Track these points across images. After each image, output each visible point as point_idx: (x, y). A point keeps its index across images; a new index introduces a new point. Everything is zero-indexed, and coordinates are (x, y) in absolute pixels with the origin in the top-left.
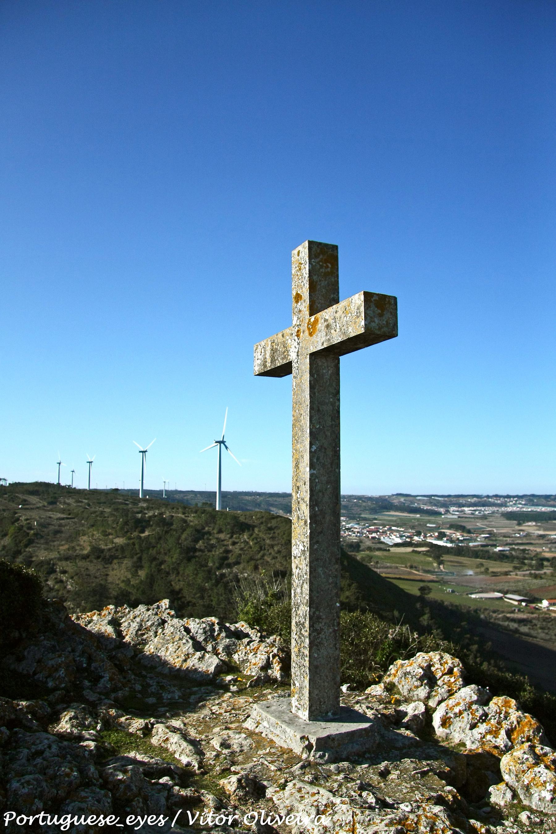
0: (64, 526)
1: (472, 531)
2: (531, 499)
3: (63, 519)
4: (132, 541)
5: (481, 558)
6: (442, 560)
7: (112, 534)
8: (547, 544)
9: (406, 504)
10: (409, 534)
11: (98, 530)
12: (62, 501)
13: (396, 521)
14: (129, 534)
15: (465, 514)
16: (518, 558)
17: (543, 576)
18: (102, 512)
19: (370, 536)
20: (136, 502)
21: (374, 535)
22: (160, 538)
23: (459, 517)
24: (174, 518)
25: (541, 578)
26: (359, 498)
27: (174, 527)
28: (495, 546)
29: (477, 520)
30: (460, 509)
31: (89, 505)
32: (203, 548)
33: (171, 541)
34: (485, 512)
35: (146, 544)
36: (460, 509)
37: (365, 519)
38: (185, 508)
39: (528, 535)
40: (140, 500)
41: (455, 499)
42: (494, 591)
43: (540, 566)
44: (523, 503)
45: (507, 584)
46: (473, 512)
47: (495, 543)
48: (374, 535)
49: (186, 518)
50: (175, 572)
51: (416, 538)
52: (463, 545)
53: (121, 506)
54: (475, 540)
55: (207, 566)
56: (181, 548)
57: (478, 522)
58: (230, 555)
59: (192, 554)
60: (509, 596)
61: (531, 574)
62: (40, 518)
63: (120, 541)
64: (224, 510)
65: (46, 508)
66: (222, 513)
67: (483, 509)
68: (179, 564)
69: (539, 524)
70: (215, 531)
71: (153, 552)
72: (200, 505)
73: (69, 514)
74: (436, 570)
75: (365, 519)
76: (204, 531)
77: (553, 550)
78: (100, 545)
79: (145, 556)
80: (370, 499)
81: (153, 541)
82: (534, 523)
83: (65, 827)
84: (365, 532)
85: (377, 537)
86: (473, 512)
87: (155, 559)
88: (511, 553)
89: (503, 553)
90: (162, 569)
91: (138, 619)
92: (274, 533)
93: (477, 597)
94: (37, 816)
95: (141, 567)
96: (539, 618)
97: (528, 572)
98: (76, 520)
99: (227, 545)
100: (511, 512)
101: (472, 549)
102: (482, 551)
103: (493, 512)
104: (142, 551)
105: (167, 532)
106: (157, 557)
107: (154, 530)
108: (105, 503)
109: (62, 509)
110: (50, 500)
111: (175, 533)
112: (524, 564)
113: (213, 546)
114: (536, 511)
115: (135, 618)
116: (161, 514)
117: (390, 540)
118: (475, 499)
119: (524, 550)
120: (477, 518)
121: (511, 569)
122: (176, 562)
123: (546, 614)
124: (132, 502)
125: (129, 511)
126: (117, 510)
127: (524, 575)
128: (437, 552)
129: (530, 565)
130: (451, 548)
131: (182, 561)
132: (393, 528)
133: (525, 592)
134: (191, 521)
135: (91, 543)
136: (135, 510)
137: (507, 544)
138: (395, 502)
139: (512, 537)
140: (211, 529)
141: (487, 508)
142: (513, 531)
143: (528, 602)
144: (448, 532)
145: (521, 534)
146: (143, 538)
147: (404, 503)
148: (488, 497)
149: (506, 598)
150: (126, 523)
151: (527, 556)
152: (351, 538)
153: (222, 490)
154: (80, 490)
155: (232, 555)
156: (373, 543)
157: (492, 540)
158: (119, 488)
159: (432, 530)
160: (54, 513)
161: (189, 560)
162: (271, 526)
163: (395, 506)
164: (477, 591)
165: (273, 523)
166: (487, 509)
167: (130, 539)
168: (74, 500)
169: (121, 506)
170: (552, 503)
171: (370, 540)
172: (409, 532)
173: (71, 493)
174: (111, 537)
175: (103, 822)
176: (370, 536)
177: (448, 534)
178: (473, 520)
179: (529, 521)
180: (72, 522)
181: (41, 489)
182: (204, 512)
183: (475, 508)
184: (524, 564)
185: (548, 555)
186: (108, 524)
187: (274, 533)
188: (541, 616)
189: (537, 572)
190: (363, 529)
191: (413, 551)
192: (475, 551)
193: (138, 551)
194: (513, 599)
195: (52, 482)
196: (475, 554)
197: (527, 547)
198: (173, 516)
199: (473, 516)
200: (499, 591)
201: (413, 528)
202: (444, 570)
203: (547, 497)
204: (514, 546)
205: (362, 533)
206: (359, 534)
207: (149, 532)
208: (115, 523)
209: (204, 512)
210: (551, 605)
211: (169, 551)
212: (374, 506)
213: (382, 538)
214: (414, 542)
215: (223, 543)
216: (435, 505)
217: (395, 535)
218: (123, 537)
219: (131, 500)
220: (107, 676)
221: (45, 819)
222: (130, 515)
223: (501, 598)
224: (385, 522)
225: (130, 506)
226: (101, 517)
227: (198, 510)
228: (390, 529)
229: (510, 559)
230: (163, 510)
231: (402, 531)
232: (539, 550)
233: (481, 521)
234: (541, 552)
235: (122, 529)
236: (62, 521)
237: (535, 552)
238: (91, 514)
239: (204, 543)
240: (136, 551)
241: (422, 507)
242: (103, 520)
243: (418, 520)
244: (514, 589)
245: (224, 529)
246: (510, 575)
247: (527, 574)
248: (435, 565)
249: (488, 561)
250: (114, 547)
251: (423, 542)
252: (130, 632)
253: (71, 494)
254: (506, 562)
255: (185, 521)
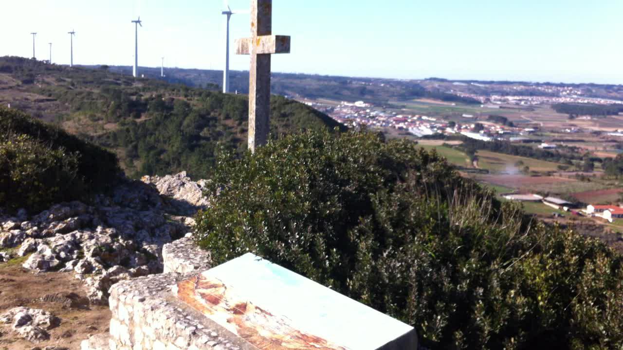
0: (44, 110)
1: (514, 123)
2: (589, 89)
3: (42, 101)
4: (126, 127)
5: (522, 155)
6: (476, 156)
7: (102, 119)
8: (602, 142)
9: (441, 91)
10: (441, 125)
11: (85, 114)
12: (40, 80)
13: (427, 109)
14: (122, 119)
15: (508, 104)
16: (565, 157)
17: (591, 179)
18: (90, 94)
19: (397, 126)
20: (130, 82)
21: (401, 125)
22: (158, 124)
23: (501, 107)
24: (174, 102)
25: (589, 180)
26: (388, 82)
27: (174, 112)
28: (540, 142)
29: (521, 111)
30: (503, 98)
31: (73, 85)
32: (208, 136)
33: (171, 127)
34: (532, 103)
35: (142, 130)
36: (503, 98)
37: (392, 107)
38: (187, 90)
39: (580, 131)
40: (133, 80)
41: (498, 86)
42: (533, 192)
43: (590, 167)
44: (579, 93)
45: (548, 186)
46: (519, 102)
47: (540, 138)
48: (401, 125)
49: (188, 102)
50: (176, 162)
51: (449, 130)
52: (502, 139)
53: (111, 87)
54: (517, 135)
55: (212, 156)
56: (183, 135)
57: (523, 114)
58: (238, 144)
59: (195, 142)
60: (549, 199)
61: (577, 176)
62: (14, 99)
63: (112, 127)
64: (231, 93)
65: (21, 88)
66: (229, 97)
67: (530, 98)
68: (180, 153)
69: (595, 119)
70: (222, 117)
71: (151, 140)
72: (204, 86)
73: (50, 95)
74: (468, 167)
75: (392, 107)
76: (209, 116)
77: (608, 149)
78: (88, 131)
79: (141, 145)
80: (399, 83)
81: (151, 127)
82: (589, 118)
84: (392, 121)
85: (405, 127)
86: (519, 102)
87: (152, 148)
88: (557, 151)
89: (550, 150)
90: (161, 159)
91: (167, 183)
92: (288, 120)
93: (513, 198)
95: (137, 157)
96: (581, 225)
97: (574, 173)
98: (58, 102)
99: (236, 133)
100: (563, 103)
101: (512, 144)
102: (524, 147)
103: (542, 103)
104: (138, 139)
105: (166, 117)
106: (156, 146)
107: (151, 115)
108: (92, 82)
109: (41, 89)
110: (25, 78)
111: (175, 118)
112: (571, 163)
113: (219, 134)
114: (594, 103)
115: (165, 182)
116: (160, 96)
117: (419, 131)
118: (522, 87)
119: (572, 149)
120: (522, 109)
121: (555, 169)
122: (177, 151)
123: (590, 220)
124: (125, 82)
125: (121, 92)
126: (107, 91)
127: (569, 177)
128: (471, 146)
129: (578, 166)
130: (488, 142)
131: (183, 151)
132: (424, 118)
133: (568, 195)
134: (194, 105)
135: (78, 129)
136: (129, 91)
137: (554, 141)
138: (429, 87)
139: (561, 133)
140: (217, 114)
141: (535, 98)
142: (564, 125)
143: (572, 206)
144: (486, 124)
145: (573, 129)
146: (138, 124)
147: (438, 90)
148: (538, 84)
149: (545, 201)
150: (119, 107)
151: (576, 155)
152: (375, 127)
153: (231, 68)
154: (60, 66)
155: (241, 144)
156: (399, 134)
157: (538, 135)
158: (108, 64)
159: (468, 121)
160: (32, 94)
161: (192, 149)
162: (285, 113)
163: (427, 92)
164: (513, 192)
165: (287, 109)
166: (534, 99)
167: (123, 124)
168: (54, 79)
169: (111, 87)
170: (614, 94)
171: (396, 130)
172: (442, 123)
173: (50, 70)
174: (100, 122)
176: (397, 126)
177: (486, 126)
178: (517, 111)
179: (583, 114)
180: (53, 104)
181: (13, 65)
182: (208, 95)
183: (521, 98)
184: (571, 163)
185: (601, 155)
186: (97, 108)
187: (288, 120)
188: (584, 223)
189: (585, 174)
190: (389, 117)
191: (445, 145)
192: (515, 146)
193: (133, 139)
194: (554, 203)
195: (25, 56)
196: (516, 150)
197: (577, 145)
198: (173, 99)
199: (517, 107)
200: (538, 193)
201: (446, 118)
202: (477, 167)
203: (609, 87)
204: (562, 143)
205: (388, 123)
206: (384, 124)
207: (146, 117)
208: (105, 106)
209: (208, 95)
210: (597, 211)
211: (169, 138)
212: (404, 91)
213: (410, 129)
214: (446, 134)
215: (230, 130)
216: (475, 92)
217: (426, 126)
218: (115, 122)
219: (124, 80)
220: (159, 204)
222: (123, 97)
223: (540, 201)
224: (416, 111)
225: (123, 86)
226: (88, 99)
227: (203, 92)
228: (420, 119)
229: (555, 158)
230: (162, 91)
231: (433, 121)
232: (591, 148)
233: (526, 113)
234: (593, 152)
235: (114, 113)
236: (42, 104)
237: (586, 152)
238: (76, 95)
239: (209, 131)
240: (131, 138)
241: (459, 94)
242: (90, 103)
243: (452, 109)
244: (557, 191)
245: (231, 114)
246: (554, 176)
247: (573, 176)
248: (468, 160)
249: (531, 159)
250: (106, 134)
251: (456, 135)
252: (163, 189)
253: (50, 72)
254: (550, 161)
255: (188, 105)
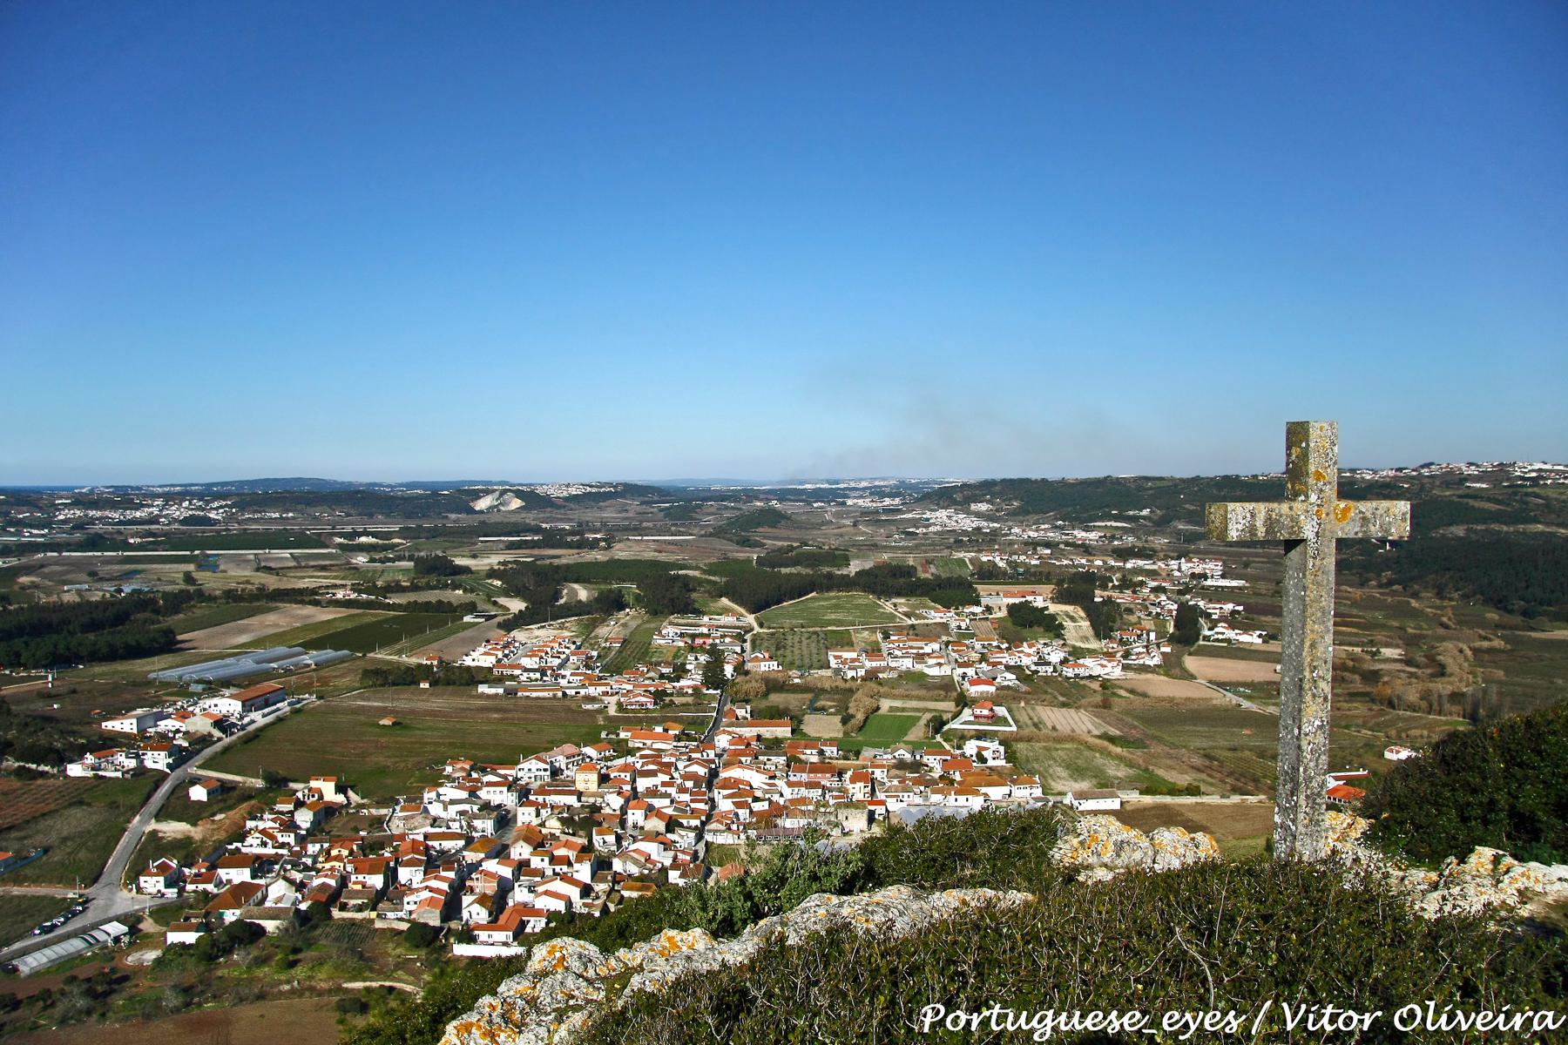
83: (1042, 1035)
94: (986, 1013)
175: (1117, 1025)
221: (1002, 1018)
